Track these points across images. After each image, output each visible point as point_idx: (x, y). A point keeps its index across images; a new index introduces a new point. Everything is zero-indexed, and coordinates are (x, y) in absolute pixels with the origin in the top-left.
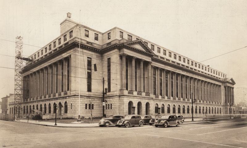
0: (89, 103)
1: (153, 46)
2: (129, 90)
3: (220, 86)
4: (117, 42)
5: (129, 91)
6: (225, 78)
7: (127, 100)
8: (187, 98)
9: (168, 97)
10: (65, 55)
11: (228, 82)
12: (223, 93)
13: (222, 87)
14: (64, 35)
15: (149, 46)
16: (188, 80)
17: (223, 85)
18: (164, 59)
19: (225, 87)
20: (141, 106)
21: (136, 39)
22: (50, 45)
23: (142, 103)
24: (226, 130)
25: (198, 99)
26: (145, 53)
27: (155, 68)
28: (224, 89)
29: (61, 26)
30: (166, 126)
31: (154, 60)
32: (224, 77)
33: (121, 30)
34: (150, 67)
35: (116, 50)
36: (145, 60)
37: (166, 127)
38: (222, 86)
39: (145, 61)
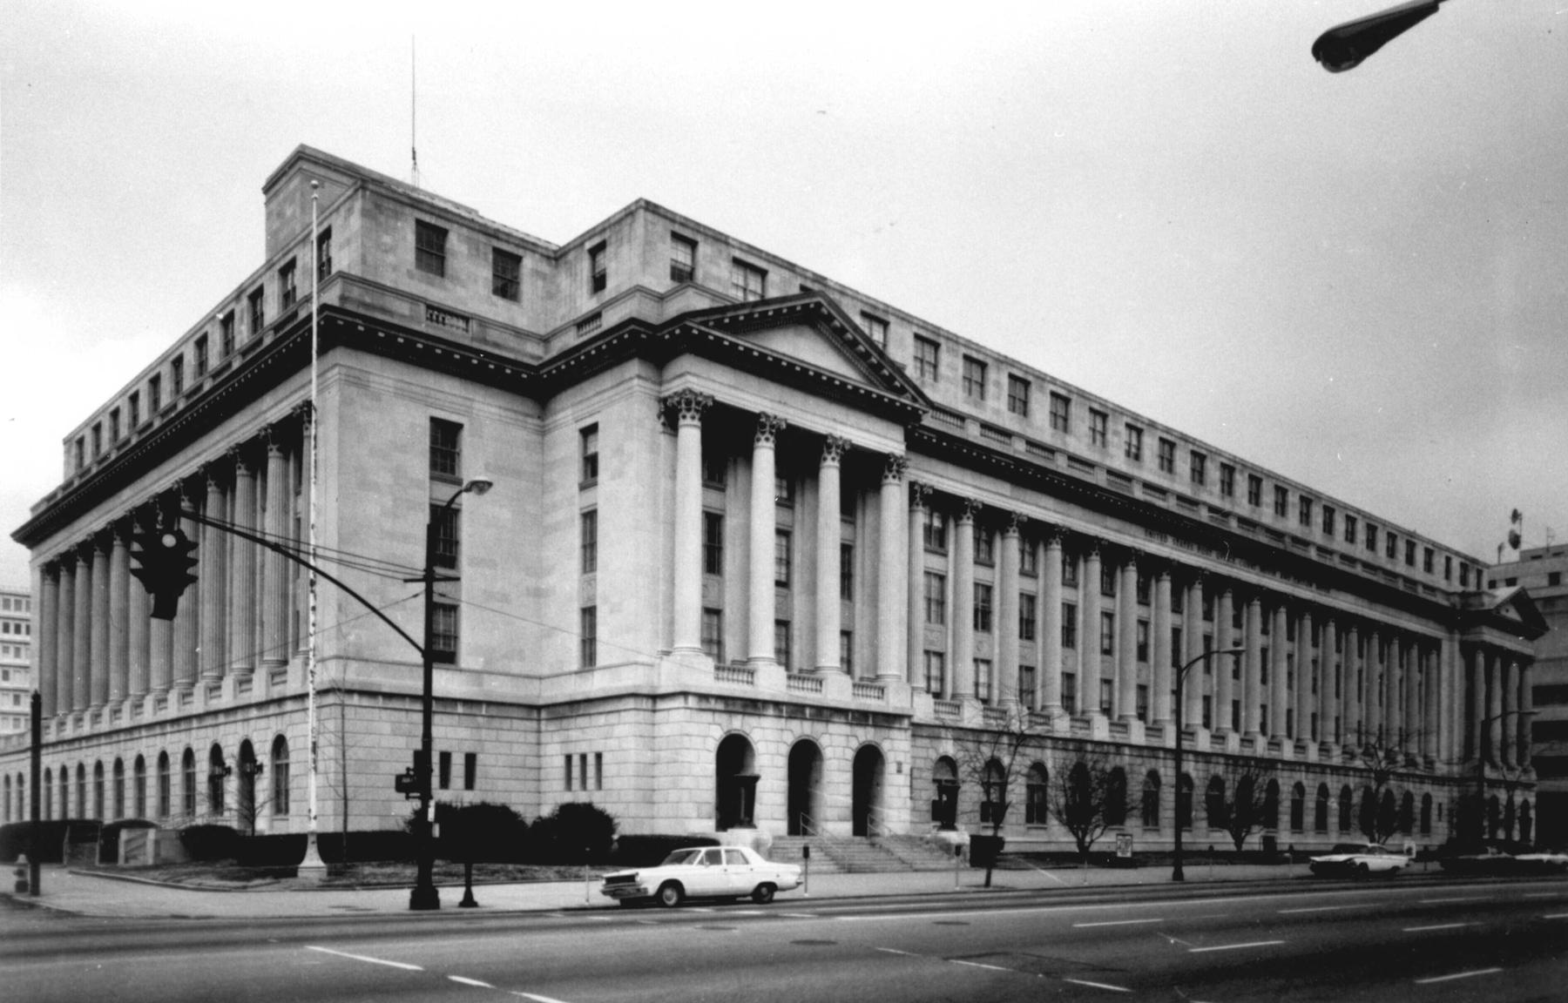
0: (469, 747)
1: (930, 340)
2: (858, 671)
3: (1430, 646)
4: (652, 314)
5: (862, 679)
6: (1472, 588)
7: (1286, 780)
8: (1289, 736)
9: (1150, 725)
10: (273, 408)
11: (1494, 619)
12: (1451, 697)
13: (1450, 650)
14: (283, 263)
15: (902, 350)
16: (1010, 548)
17: (1451, 640)
18: (1283, 542)
19: (1468, 651)
20: (820, 771)
21: (796, 291)
22: (202, 343)
23: (828, 753)
24: (1424, 924)
25: (1314, 739)
26: (856, 389)
27: (946, 507)
28: (1459, 664)
29: (267, 203)
30: (669, 899)
31: (925, 444)
32: (1464, 581)
33: (925, 325)
34: (894, 495)
35: (634, 368)
36: (720, 397)
37: (672, 902)
38: (1445, 647)
39: (790, 426)
